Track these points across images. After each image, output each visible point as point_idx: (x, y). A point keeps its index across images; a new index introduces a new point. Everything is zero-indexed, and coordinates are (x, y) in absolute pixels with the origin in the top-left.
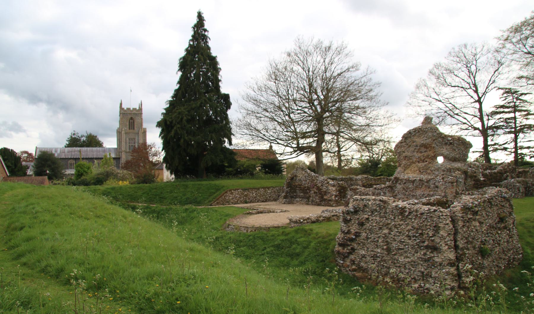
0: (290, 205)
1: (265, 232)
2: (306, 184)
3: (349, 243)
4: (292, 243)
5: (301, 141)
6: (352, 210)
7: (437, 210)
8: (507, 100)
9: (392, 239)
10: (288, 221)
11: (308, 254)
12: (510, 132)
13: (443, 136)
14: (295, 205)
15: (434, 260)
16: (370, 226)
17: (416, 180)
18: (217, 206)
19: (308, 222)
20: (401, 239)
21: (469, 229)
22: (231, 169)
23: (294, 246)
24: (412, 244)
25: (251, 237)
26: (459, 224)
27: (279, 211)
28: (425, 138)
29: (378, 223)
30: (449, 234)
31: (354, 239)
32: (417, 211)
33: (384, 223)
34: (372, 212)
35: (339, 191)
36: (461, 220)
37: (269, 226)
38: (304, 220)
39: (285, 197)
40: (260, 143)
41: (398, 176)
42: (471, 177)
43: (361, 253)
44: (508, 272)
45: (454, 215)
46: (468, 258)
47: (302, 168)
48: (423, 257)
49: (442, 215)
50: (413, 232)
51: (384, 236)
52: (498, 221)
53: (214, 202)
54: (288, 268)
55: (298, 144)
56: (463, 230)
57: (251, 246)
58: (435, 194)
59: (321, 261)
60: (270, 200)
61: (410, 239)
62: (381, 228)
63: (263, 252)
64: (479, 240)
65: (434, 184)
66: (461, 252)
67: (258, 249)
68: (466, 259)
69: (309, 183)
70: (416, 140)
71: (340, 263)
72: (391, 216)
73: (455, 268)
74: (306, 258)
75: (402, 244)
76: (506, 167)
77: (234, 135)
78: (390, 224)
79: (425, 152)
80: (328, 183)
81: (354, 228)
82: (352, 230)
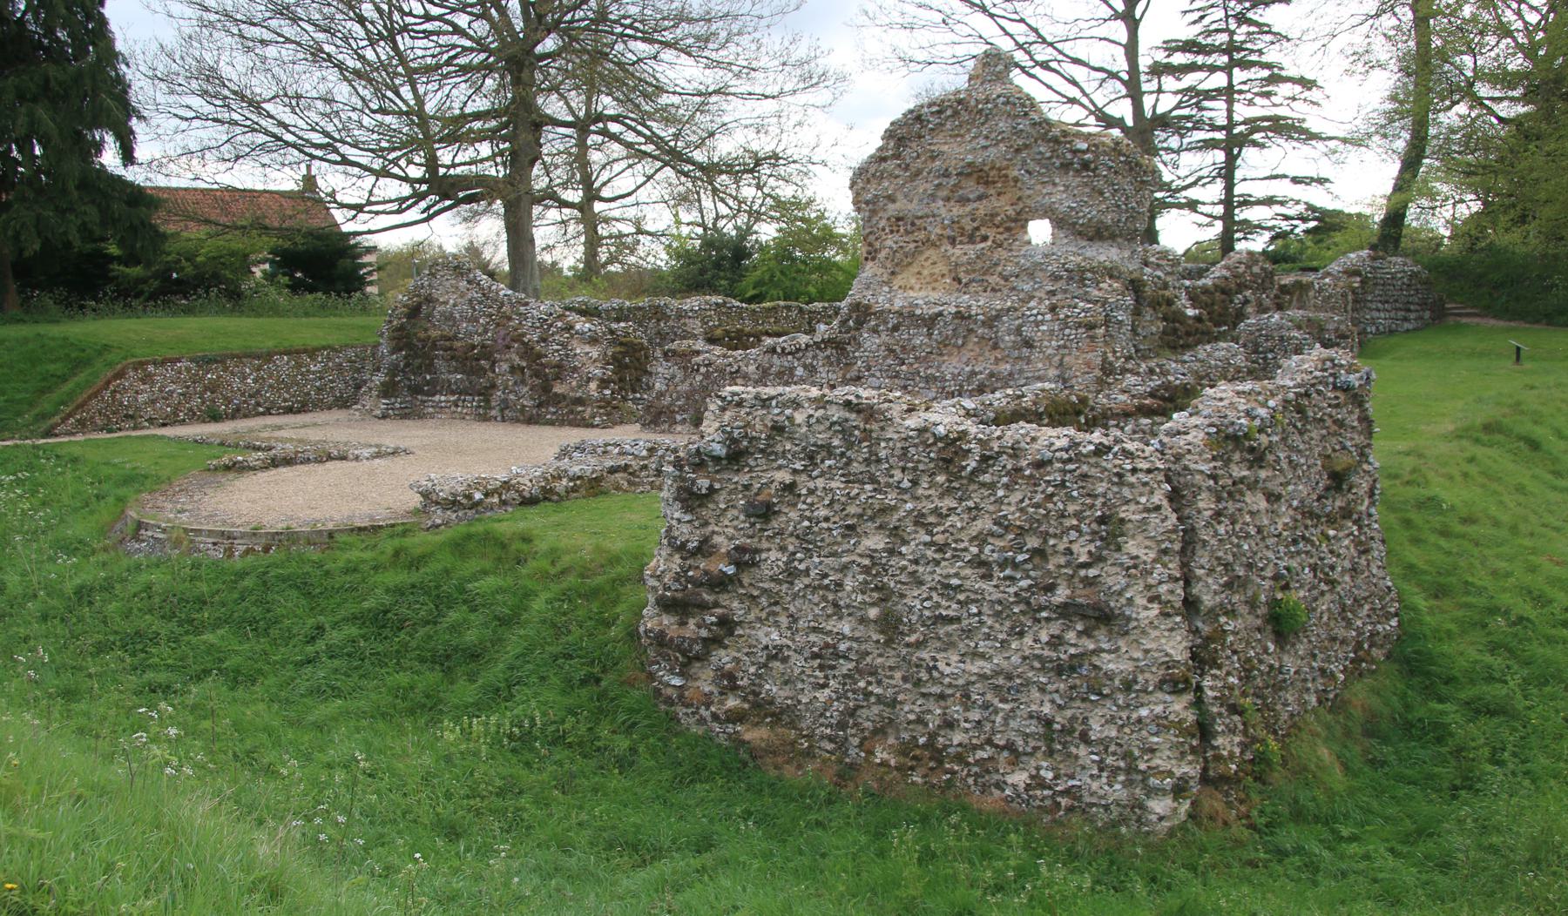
0: (407, 422)
1: (314, 554)
2: (473, 333)
3: (708, 597)
4: (442, 602)
5: (445, 156)
6: (719, 450)
7: (1109, 448)
8: (1206, 21)
9: (903, 578)
10: (416, 500)
11: (518, 650)
12: (1209, 145)
13: (1056, 132)
14: (430, 422)
15: (1096, 667)
16: (803, 517)
17: (940, 314)
18: (80, 438)
19: (504, 503)
20: (948, 576)
21: (1237, 527)
22: (136, 271)
23: (453, 616)
24: (996, 596)
25: (248, 582)
26: (1201, 505)
27: (366, 453)
28: (983, 142)
29: (837, 507)
30: (1165, 552)
31: (731, 579)
32: (1015, 451)
33: (865, 506)
34: (811, 457)
35: (616, 360)
36: (1209, 489)
37: (330, 526)
38: (487, 495)
39: (388, 390)
40: (266, 159)
41: (868, 298)
42: (1155, 304)
43: (765, 641)
44: (1360, 694)
45: (1177, 467)
46: (1235, 652)
47: (456, 268)
48: (1046, 653)
49: (1134, 471)
50: (1000, 543)
51: (867, 562)
52: (1327, 489)
53: (64, 420)
54: (434, 722)
55: (432, 163)
56: (1216, 533)
57: (253, 621)
58: (1021, 371)
59: (584, 682)
60: (319, 406)
61: (987, 577)
62: (851, 528)
63: (309, 649)
64: (1269, 573)
65: (1018, 331)
66: (1206, 629)
67: (288, 637)
68: (1228, 658)
69: (486, 331)
70: (945, 148)
71: (668, 685)
72: (898, 475)
73: (1189, 697)
74: (511, 668)
75: (950, 599)
76: (1242, 269)
77: (141, 118)
78: (894, 508)
79: (980, 198)
80: (569, 328)
81: (730, 531)
82: (717, 539)
